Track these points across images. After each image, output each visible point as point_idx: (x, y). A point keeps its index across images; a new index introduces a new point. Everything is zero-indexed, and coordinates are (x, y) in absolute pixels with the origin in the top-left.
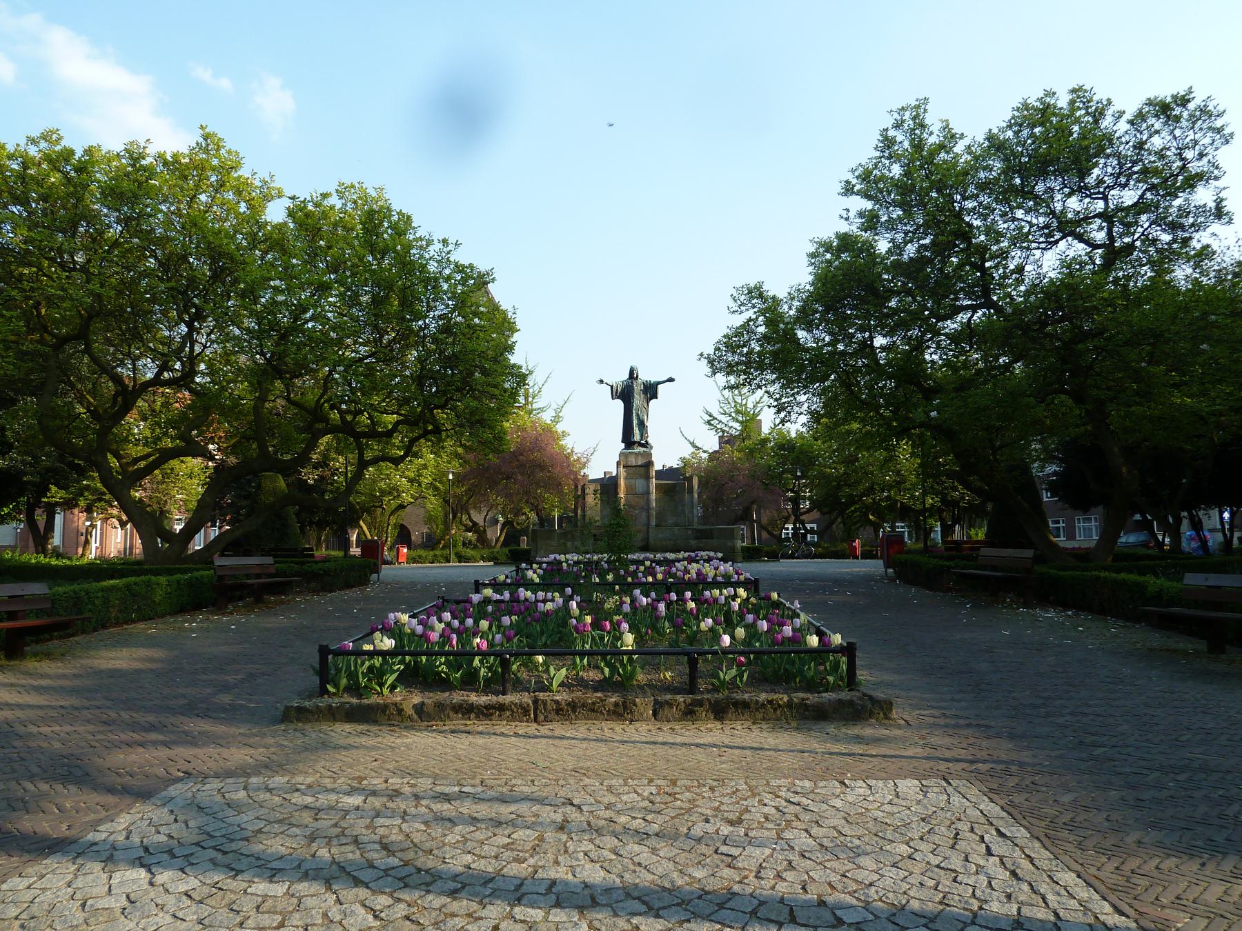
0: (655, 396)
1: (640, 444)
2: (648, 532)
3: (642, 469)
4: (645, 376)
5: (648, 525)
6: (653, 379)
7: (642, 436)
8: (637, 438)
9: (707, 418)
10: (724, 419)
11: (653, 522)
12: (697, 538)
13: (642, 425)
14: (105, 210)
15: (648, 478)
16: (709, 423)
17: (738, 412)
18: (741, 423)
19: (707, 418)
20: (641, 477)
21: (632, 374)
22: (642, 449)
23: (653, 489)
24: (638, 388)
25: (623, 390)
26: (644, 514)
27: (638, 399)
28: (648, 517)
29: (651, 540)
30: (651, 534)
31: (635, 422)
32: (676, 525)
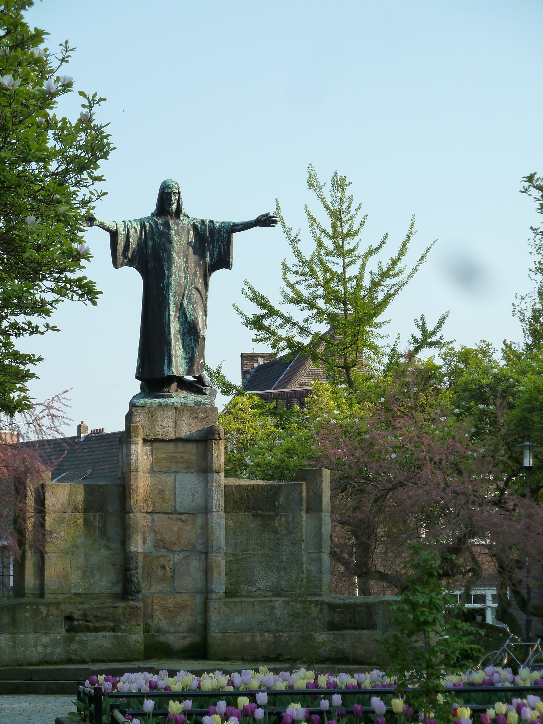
0: (223, 261)
1: (183, 384)
2: (205, 610)
3: (192, 448)
4: (200, 206)
5: (206, 592)
6: (220, 215)
7: (191, 362)
8: (178, 367)
9: (254, 310)
10: (298, 314)
11: (219, 585)
12: (332, 627)
13: (193, 335)
14: (214, 484)
15: (205, 470)
16: (256, 323)
17: (332, 296)
18: (332, 319)
19: (254, 310)
20: (188, 468)
21: (167, 202)
22: (191, 398)
23: (218, 500)
24: (181, 240)
25: (142, 245)
26: (195, 565)
27: (181, 267)
28: (207, 571)
29: (215, 633)
30: (214, 616)
31: (174, 326)
32: (278, 592)
